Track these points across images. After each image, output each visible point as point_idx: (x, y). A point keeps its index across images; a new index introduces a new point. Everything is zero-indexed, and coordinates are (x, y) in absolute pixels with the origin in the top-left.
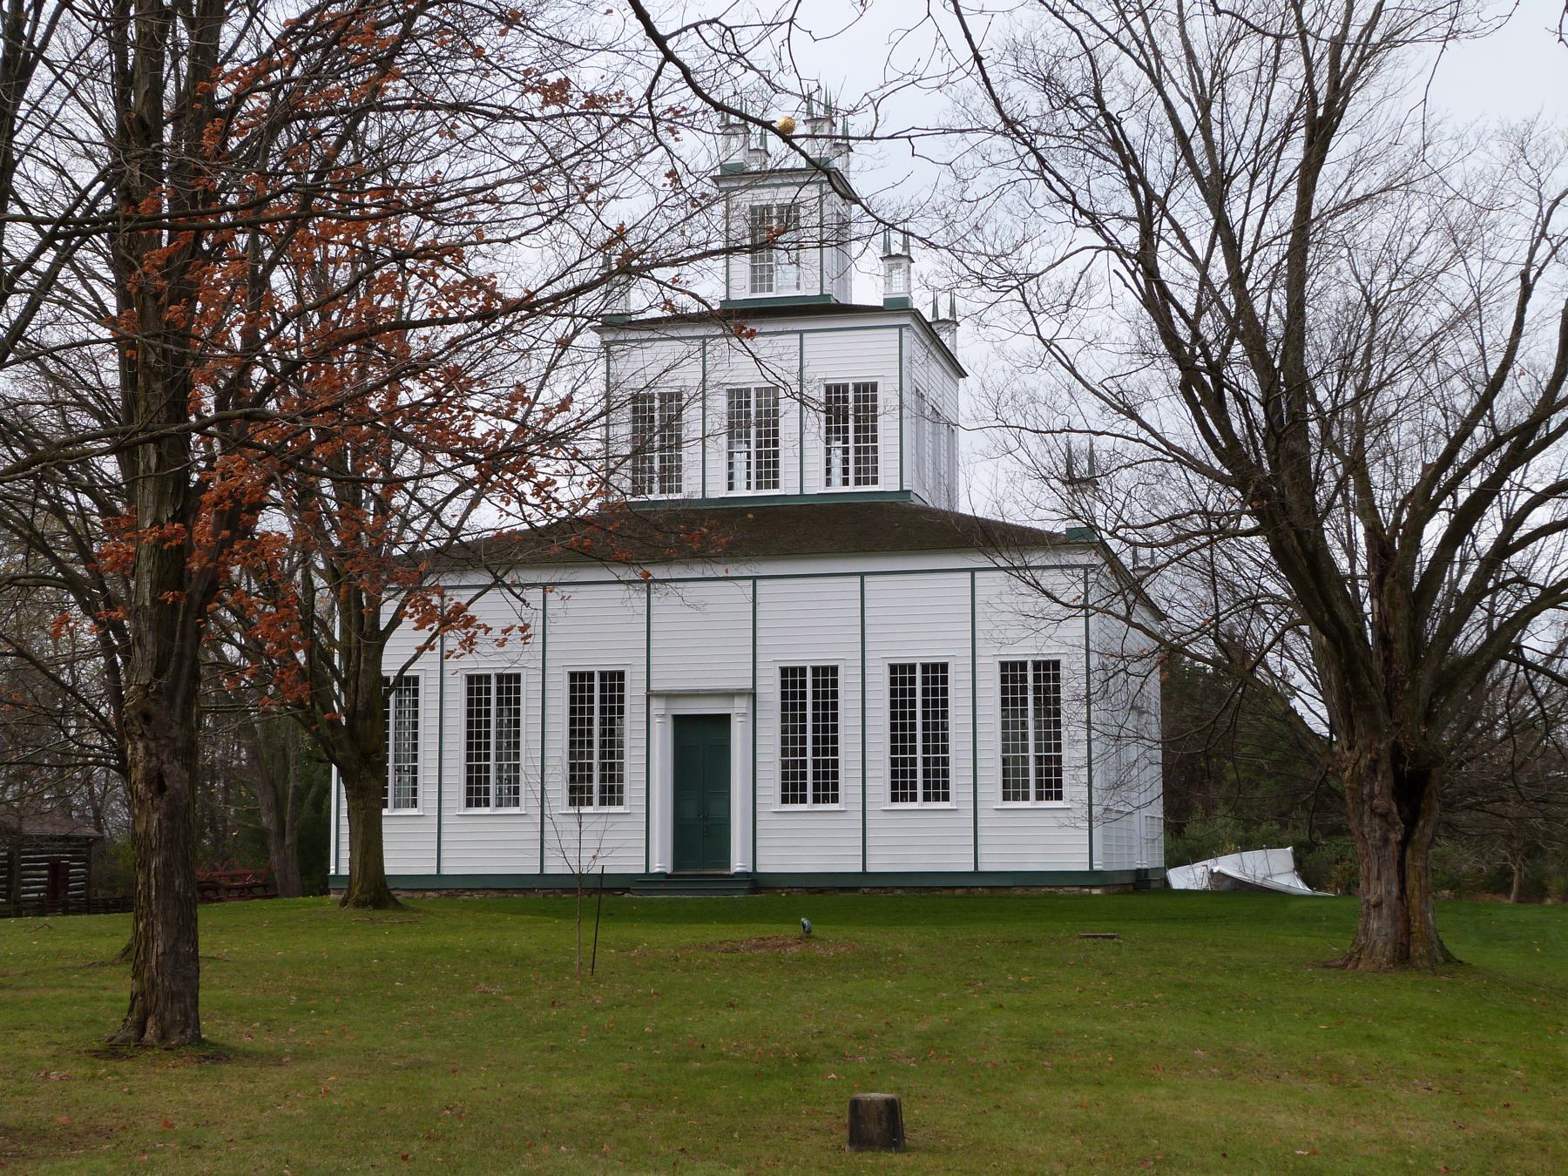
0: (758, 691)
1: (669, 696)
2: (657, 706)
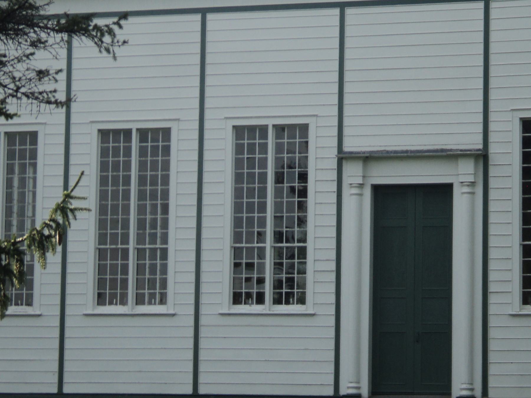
0: (493, 149)
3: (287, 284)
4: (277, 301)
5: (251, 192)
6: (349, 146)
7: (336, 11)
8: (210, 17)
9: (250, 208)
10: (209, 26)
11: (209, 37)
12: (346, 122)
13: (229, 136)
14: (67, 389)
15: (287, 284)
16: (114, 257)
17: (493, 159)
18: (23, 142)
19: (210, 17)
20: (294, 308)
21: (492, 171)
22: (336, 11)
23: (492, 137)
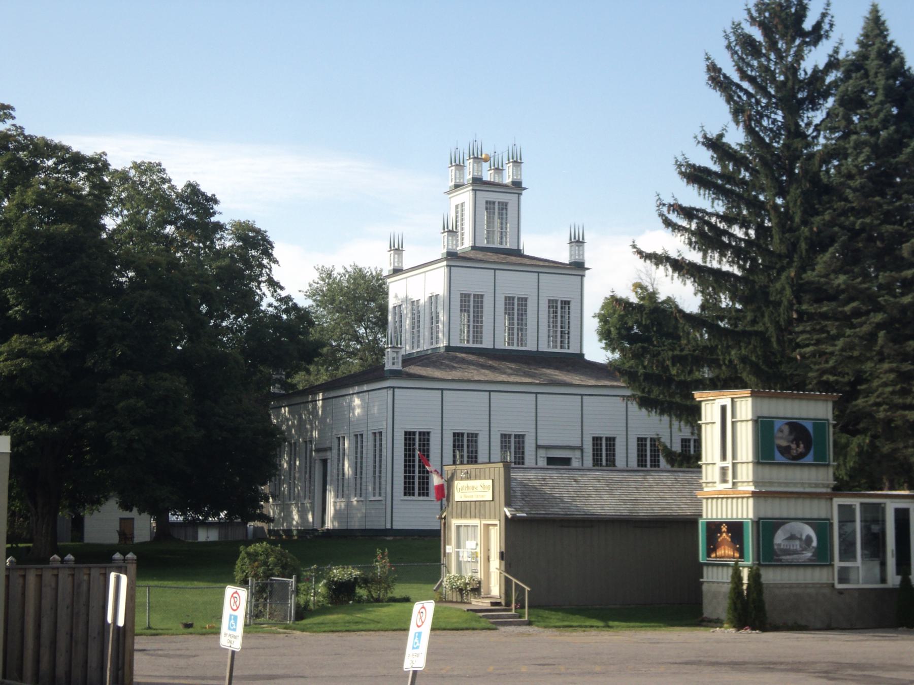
0: (584, 447)
1: (547, 448)
2: (542, 453)
3: (897, 486)
4: (419, 495)
5: (410, 456)
6: (540, 443)
7: (488, 393)
8: (396, 390)
9: (410, 461)
10: (538, 399)
11: (534, 403)
12: (538, 435)
13: (679, 441)
14: (394, 527)
15: (897, 486)
16: (409, 478)
17: (585, 450)
18: (410, 435)
19: (396, 390)
20: (425, 498)
21: (584, 454)
22: (440, 392)
23: (584, 443)
